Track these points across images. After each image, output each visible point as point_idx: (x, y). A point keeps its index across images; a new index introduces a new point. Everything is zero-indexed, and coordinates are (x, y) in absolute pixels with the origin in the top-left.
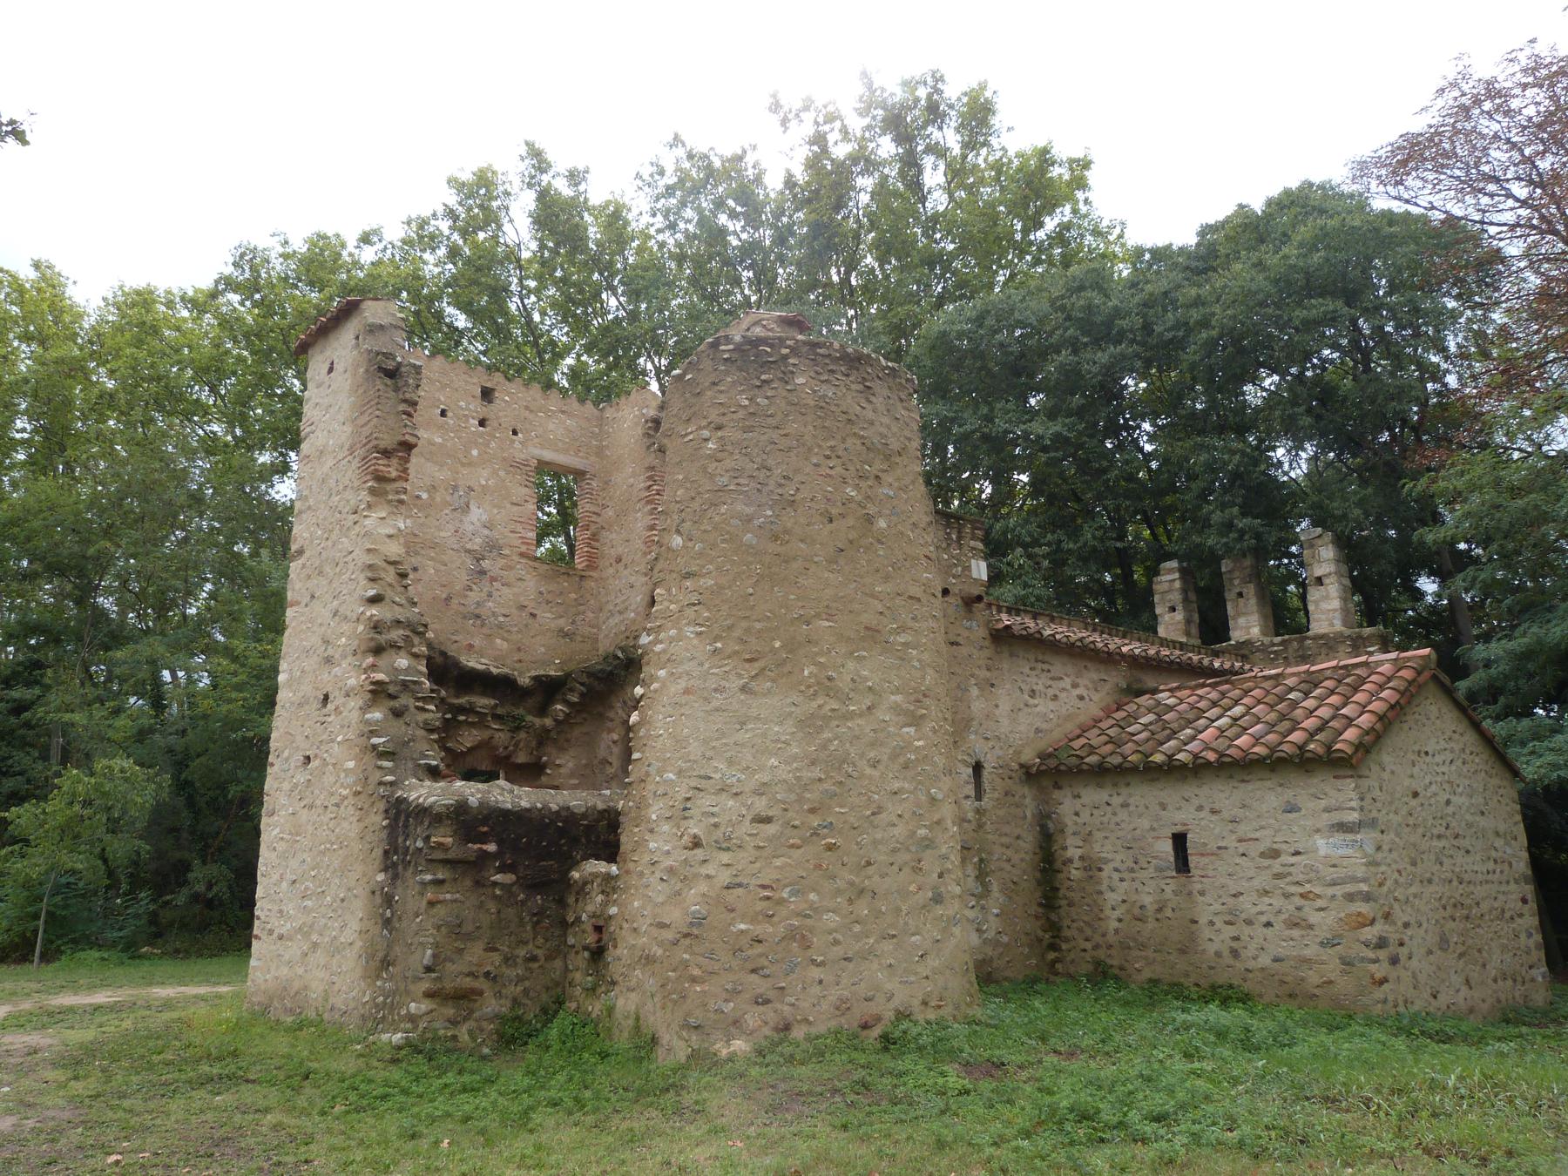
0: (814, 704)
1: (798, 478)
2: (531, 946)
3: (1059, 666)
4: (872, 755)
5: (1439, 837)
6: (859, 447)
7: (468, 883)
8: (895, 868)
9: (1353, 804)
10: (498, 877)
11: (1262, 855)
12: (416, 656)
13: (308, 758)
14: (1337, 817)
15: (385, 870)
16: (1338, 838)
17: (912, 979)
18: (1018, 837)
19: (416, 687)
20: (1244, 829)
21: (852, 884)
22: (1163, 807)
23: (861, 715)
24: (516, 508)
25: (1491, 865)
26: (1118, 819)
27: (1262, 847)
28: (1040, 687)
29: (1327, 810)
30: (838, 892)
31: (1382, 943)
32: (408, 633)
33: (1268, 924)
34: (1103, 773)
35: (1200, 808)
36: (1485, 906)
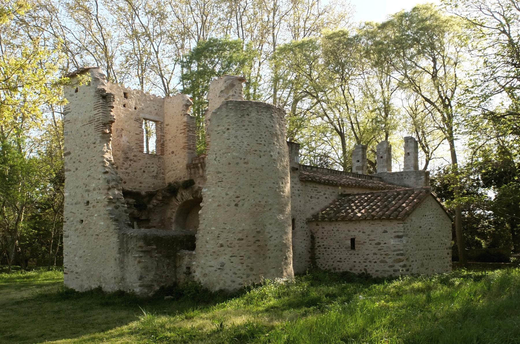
3: (320, 188)
5: (426, 238)
6: (269, 135)
7: (148, 257)
9: (402, 231)
11: (376, 244)
13: (82, 221)
14: (397, 234)
15: (120, 253)
16: (397, 239)
20: (372, 237)
22: (349, 231)
24: (137, 135)
25: (440, 245)
27: (376, 242)
29: (395, 232)
31: (404, 266)
33: (375, 262)
35: (360, 231)
36: (436, 256)
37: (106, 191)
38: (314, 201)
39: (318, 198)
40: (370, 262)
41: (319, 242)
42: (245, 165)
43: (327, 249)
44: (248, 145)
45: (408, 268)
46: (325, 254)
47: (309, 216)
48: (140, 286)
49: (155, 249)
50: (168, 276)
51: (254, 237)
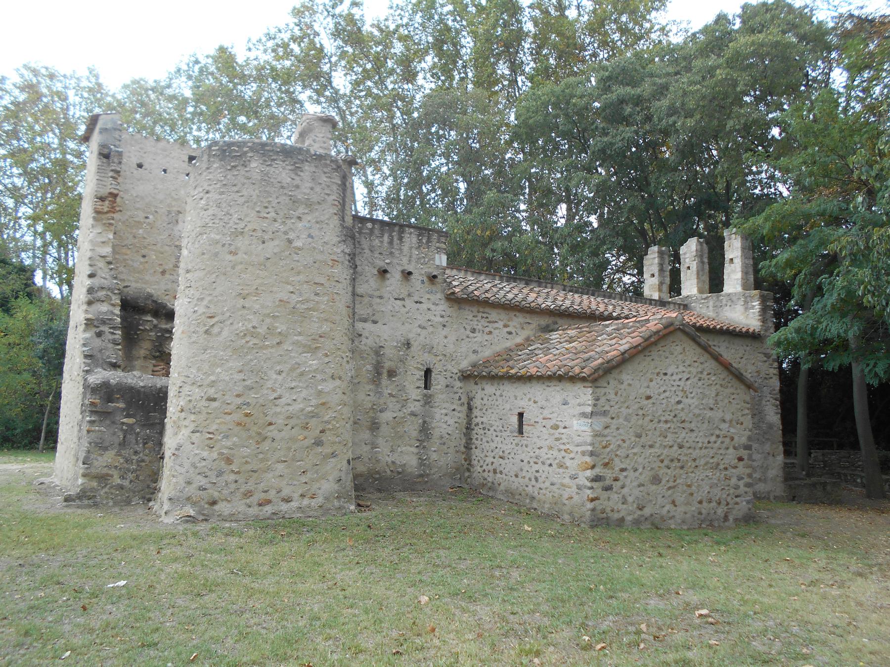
0: (244, 341)
1: (248, 219)
2: (141, 455)
3: (494, 315)
4: (278, 368)
8: (289, 427)
10: (125, 420)
12: (113, 305)
17: (295, 483)
18: (454, 410)
19: (111, 322)
20: (546, 413)
21: (259, 434)
23: (272, 347)
26: (497, 403)
28: (480, 327)
29: (579, 405)
30: (250, 437)
32: (109, 293)
33: (551, 465)
34: (493, 378)
35: (530, 400)
37: (85, 307)
38: (479, 337)
39: (490, 333)
40: (543, 463)
41: (479, 417)
42: (230, 257)
43: (486, 431)
44: (240, 219)
45: (608, 482)
46: (484, 440)
47: (465, 364)
48: (84, 475)
49: (124, 410)
50: (143, 461)
51: (238, 396)
